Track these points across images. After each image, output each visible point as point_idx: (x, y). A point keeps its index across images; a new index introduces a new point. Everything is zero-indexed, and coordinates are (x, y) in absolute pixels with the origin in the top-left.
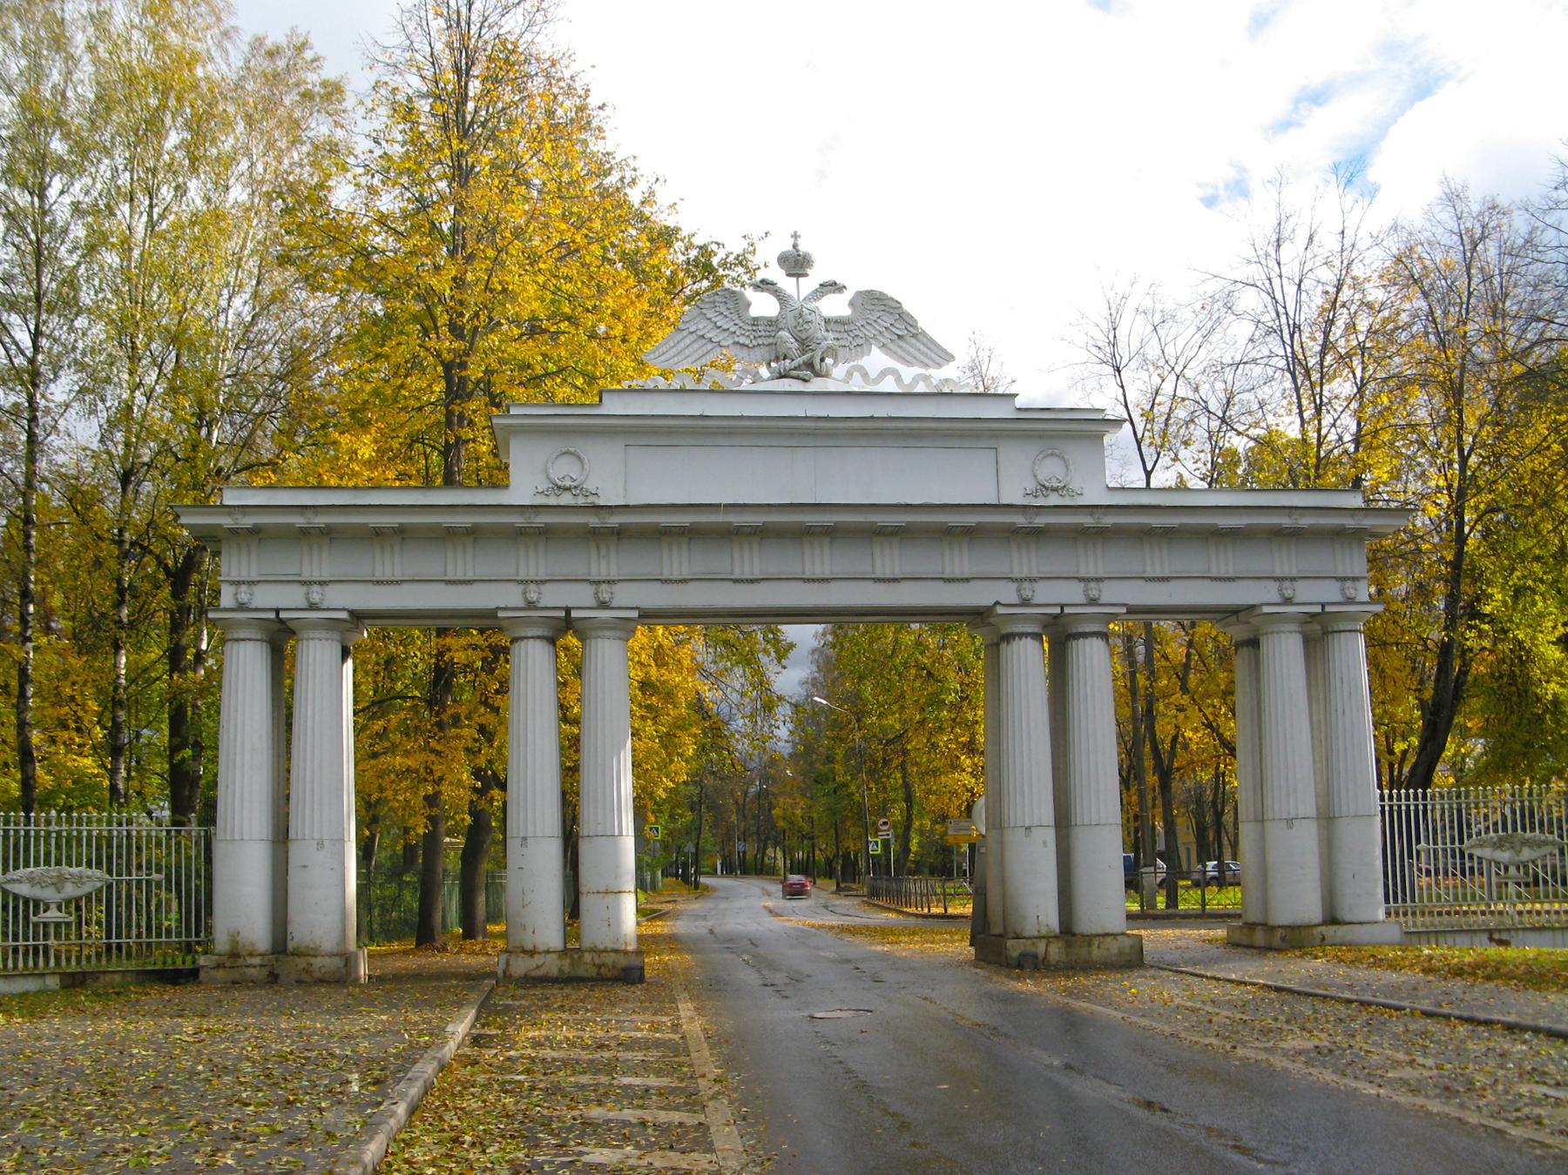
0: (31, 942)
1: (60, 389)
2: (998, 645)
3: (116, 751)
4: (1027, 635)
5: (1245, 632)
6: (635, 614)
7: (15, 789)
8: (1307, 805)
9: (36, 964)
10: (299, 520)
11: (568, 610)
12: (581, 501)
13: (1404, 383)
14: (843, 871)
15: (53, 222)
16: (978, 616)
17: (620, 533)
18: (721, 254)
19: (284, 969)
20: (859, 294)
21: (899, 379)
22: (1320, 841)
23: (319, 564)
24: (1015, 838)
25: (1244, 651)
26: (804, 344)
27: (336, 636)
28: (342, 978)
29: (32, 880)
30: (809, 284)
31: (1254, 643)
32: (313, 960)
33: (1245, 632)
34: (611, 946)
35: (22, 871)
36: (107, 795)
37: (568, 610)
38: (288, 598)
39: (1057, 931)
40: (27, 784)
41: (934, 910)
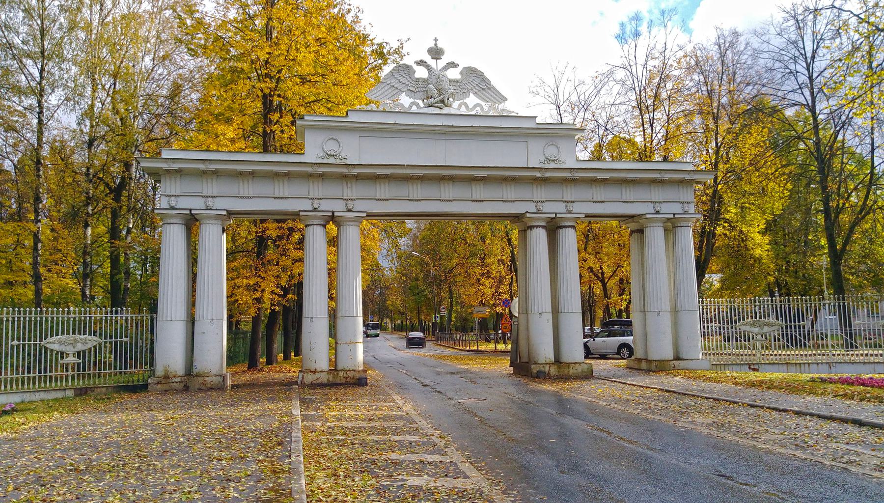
0: (59, 373)
1: (54, 99)
2: (525, 231)
3: (85, 276)
4: (540, 226)
5: (637, 227)
6: (364, 215)
7: (31, 295)
8: (666, 305)
9: (56, 385)
10: (202, 167)
11: (333, 212)
12: (338, 162)
13: (691, 113)
14: (441, 332)
15: (49, 15)
16: (517, 218)
17: (357, 177)
18: (388, 48)
19: (191, 384)
20: (464, 68)
21: (482, 108)
22: (188, 279)
23: (212, 187)
24: (534, 319)
25: (635, 235)
26: (440, 91)
27: (220, 222)
28: (220, 388)
29: (60, 342)
30: (442, 63)
31: (641, 231)
32: (206, 379)
33: (637, 227)
34: (352, 368)
35: (55, 338)
36: (80, 298)
37: (333, 212)
38: (196, 204)
39: (553, 360)
40: (38, 292)
41: (472, 348)
